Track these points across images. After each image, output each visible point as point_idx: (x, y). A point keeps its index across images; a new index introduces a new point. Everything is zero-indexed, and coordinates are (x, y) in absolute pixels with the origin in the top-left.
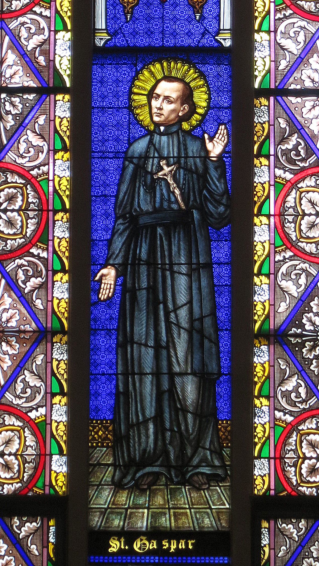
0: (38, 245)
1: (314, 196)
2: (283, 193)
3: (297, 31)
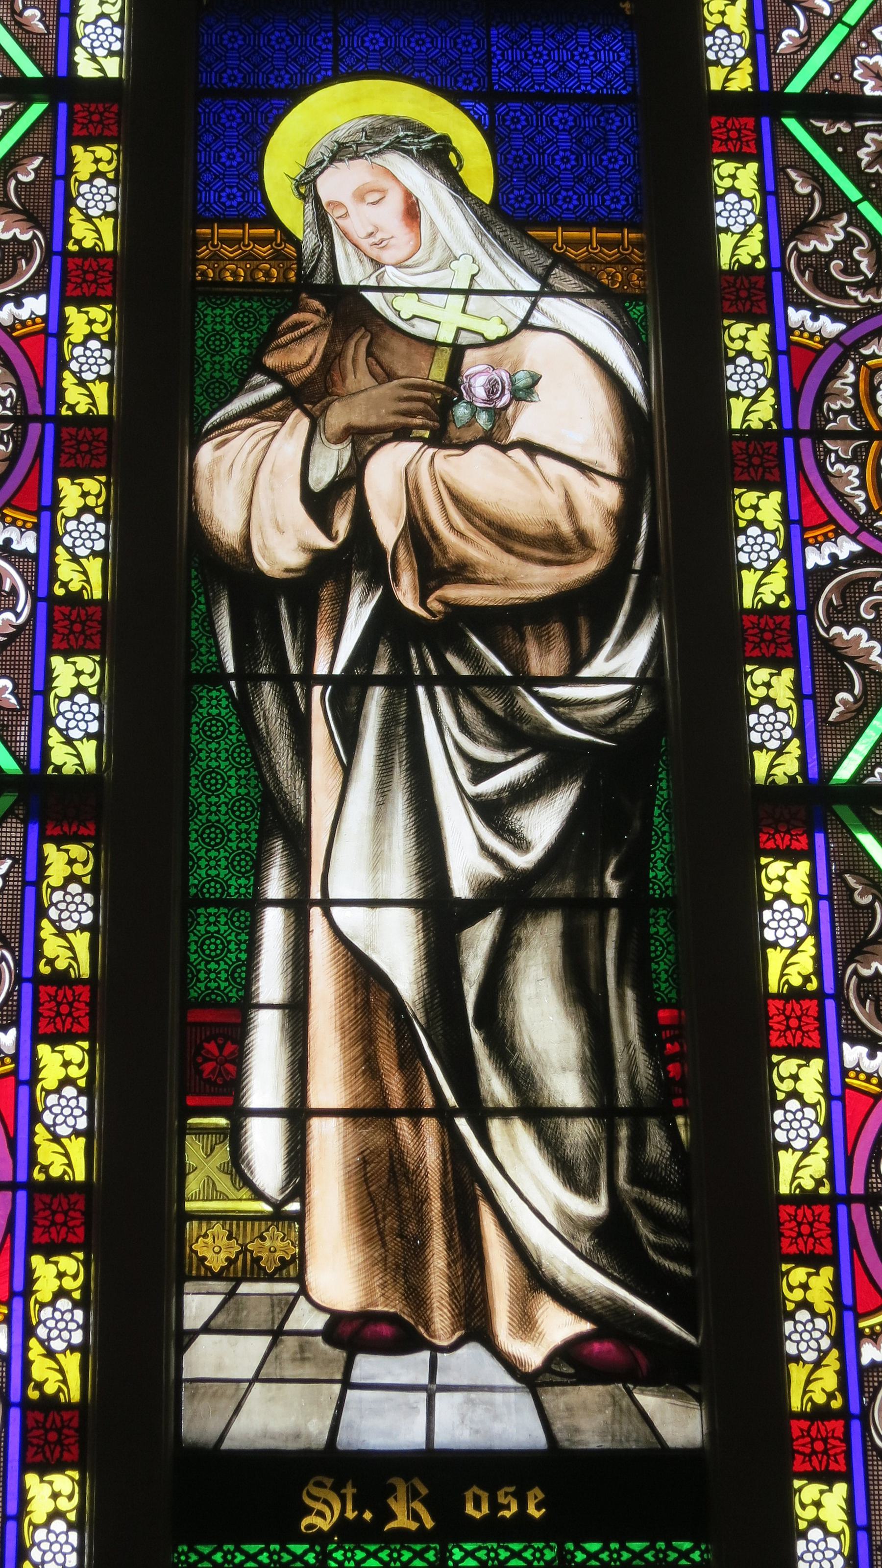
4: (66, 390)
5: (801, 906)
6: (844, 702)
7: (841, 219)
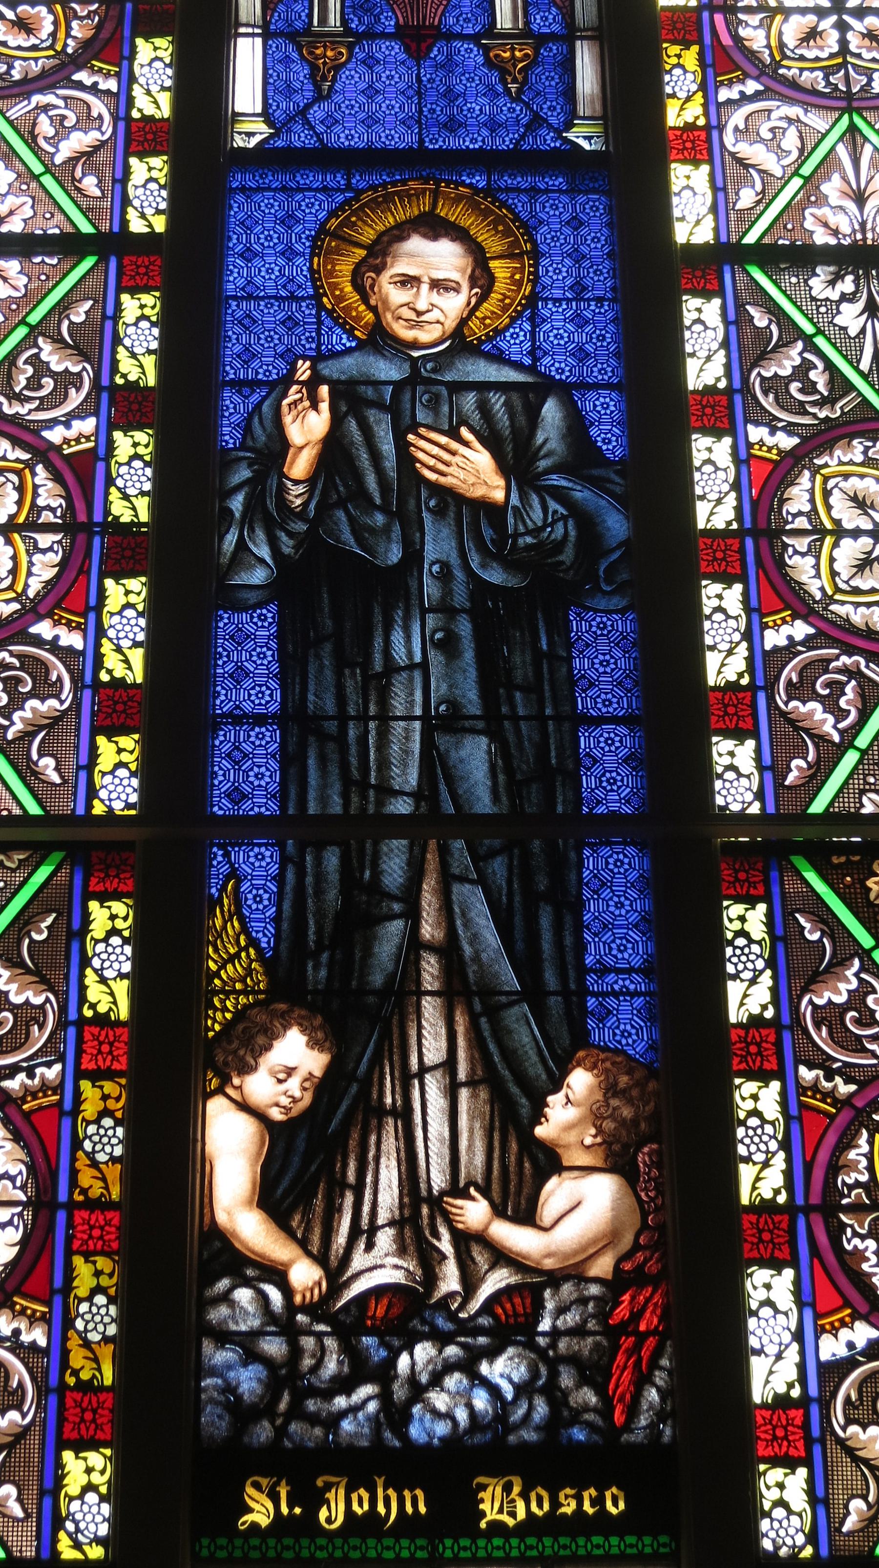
0: (94, 66)
1: (866, 486)
2: (831, 1139)
3: (779, 128)
4: (87, 987)
6: (799, 768)
7: (852, 965)
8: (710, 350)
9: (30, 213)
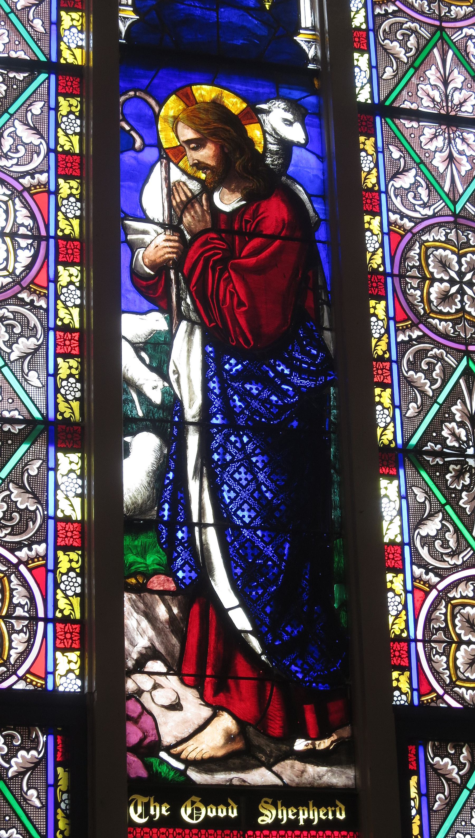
5: (382, 320)
6: (413, 408)
8: (357, 8)
9: (7, 40)
